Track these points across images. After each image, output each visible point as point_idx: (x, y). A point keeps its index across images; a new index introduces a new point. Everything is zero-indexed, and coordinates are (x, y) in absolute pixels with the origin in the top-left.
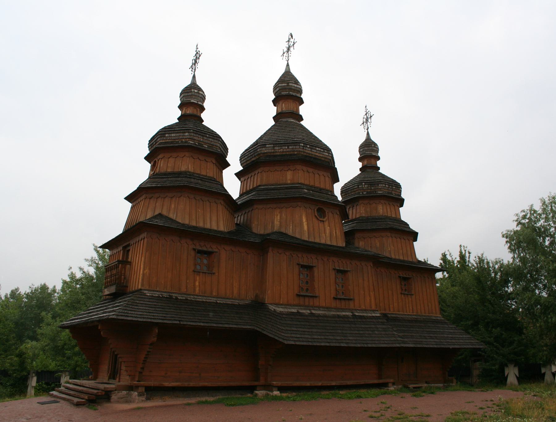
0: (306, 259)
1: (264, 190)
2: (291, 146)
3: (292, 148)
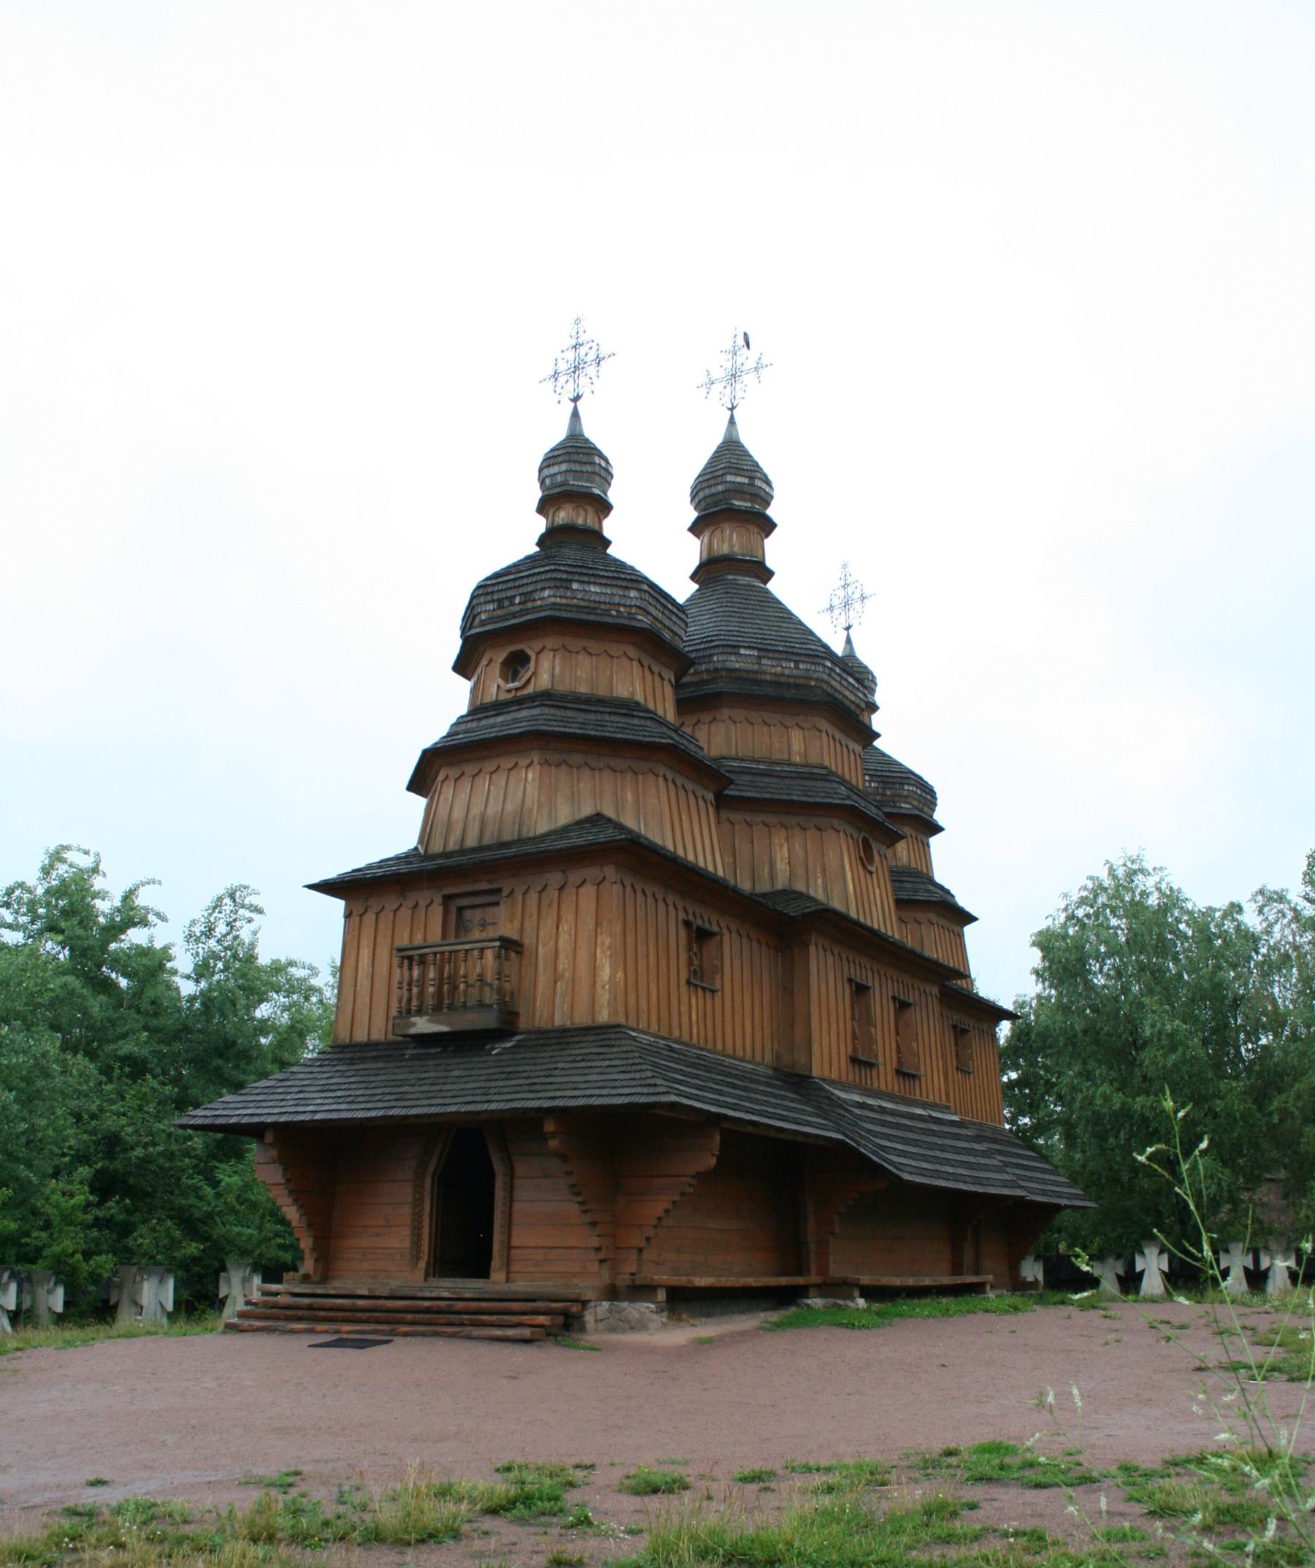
1: (743, 773)
2: (803, 662)
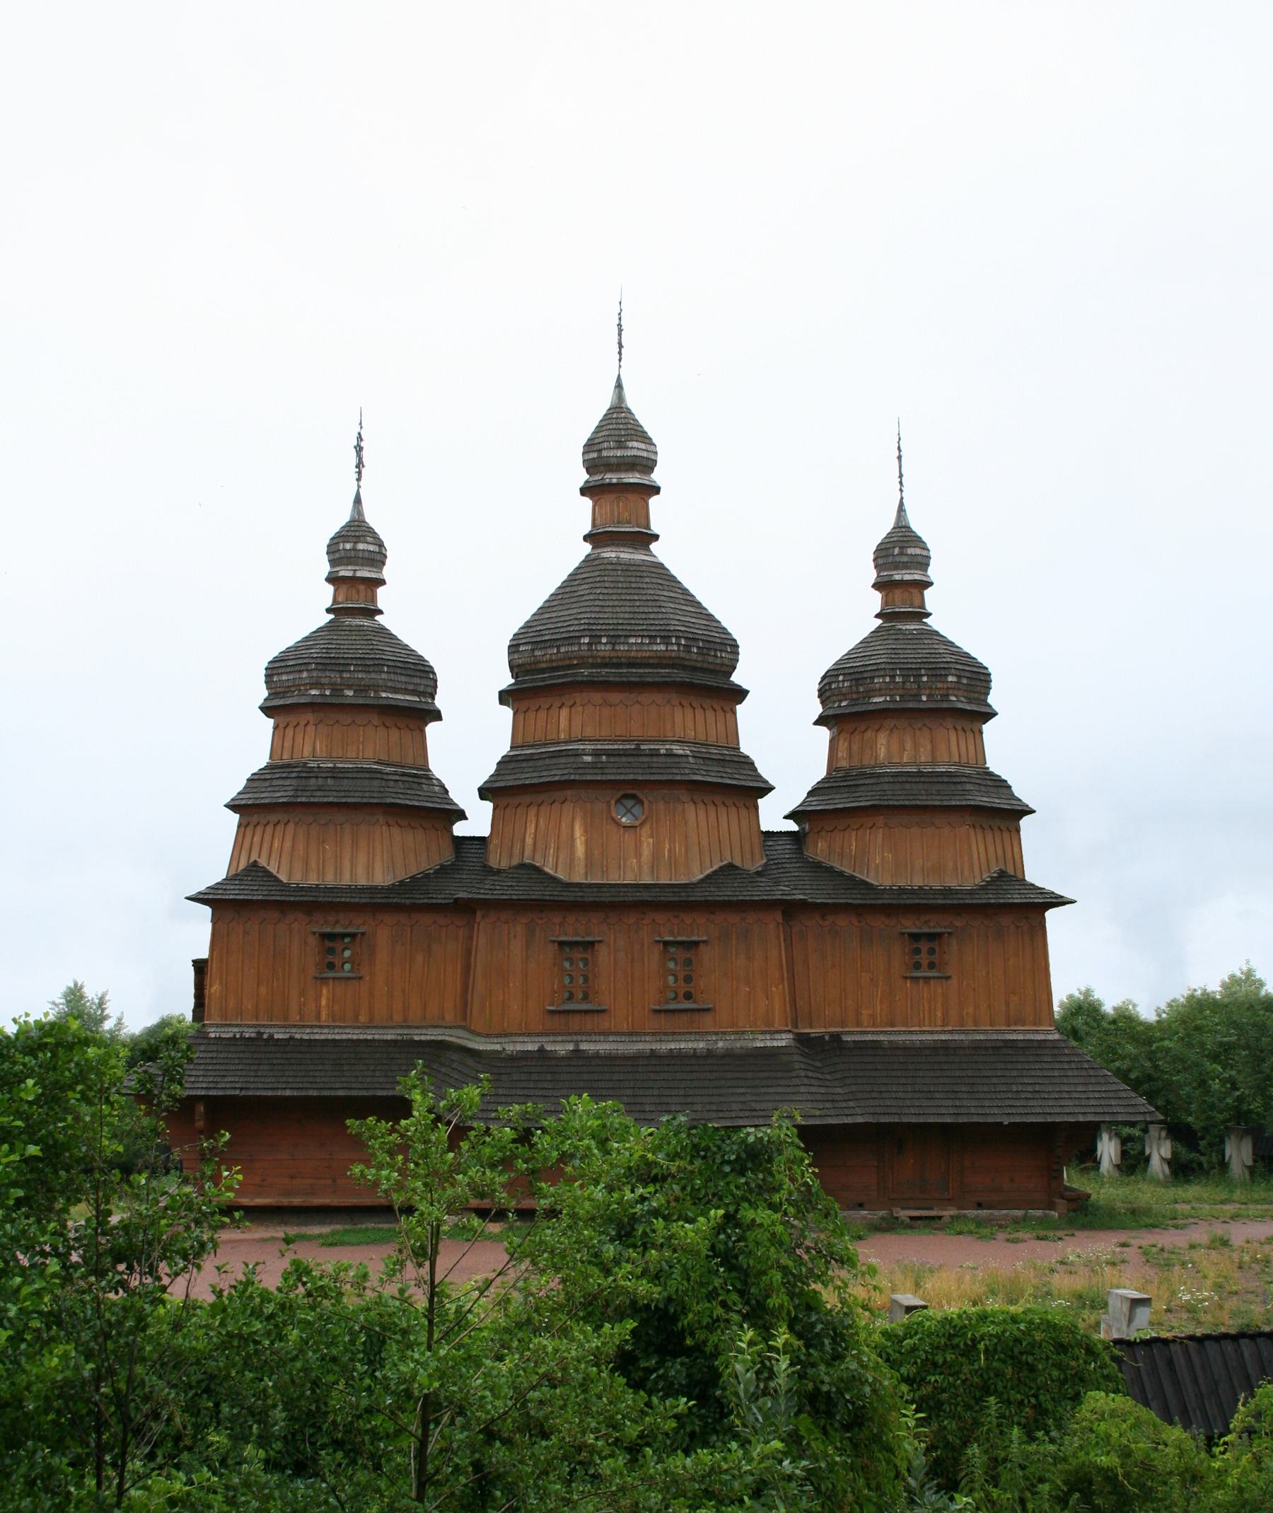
0: (573, 928)
3: (567, 652)
